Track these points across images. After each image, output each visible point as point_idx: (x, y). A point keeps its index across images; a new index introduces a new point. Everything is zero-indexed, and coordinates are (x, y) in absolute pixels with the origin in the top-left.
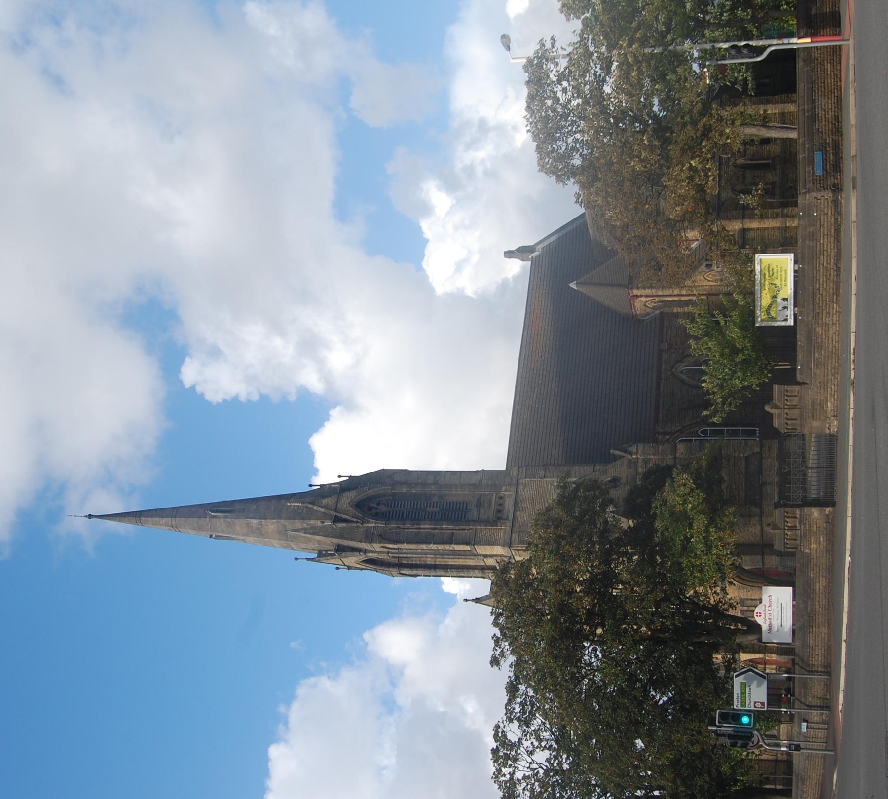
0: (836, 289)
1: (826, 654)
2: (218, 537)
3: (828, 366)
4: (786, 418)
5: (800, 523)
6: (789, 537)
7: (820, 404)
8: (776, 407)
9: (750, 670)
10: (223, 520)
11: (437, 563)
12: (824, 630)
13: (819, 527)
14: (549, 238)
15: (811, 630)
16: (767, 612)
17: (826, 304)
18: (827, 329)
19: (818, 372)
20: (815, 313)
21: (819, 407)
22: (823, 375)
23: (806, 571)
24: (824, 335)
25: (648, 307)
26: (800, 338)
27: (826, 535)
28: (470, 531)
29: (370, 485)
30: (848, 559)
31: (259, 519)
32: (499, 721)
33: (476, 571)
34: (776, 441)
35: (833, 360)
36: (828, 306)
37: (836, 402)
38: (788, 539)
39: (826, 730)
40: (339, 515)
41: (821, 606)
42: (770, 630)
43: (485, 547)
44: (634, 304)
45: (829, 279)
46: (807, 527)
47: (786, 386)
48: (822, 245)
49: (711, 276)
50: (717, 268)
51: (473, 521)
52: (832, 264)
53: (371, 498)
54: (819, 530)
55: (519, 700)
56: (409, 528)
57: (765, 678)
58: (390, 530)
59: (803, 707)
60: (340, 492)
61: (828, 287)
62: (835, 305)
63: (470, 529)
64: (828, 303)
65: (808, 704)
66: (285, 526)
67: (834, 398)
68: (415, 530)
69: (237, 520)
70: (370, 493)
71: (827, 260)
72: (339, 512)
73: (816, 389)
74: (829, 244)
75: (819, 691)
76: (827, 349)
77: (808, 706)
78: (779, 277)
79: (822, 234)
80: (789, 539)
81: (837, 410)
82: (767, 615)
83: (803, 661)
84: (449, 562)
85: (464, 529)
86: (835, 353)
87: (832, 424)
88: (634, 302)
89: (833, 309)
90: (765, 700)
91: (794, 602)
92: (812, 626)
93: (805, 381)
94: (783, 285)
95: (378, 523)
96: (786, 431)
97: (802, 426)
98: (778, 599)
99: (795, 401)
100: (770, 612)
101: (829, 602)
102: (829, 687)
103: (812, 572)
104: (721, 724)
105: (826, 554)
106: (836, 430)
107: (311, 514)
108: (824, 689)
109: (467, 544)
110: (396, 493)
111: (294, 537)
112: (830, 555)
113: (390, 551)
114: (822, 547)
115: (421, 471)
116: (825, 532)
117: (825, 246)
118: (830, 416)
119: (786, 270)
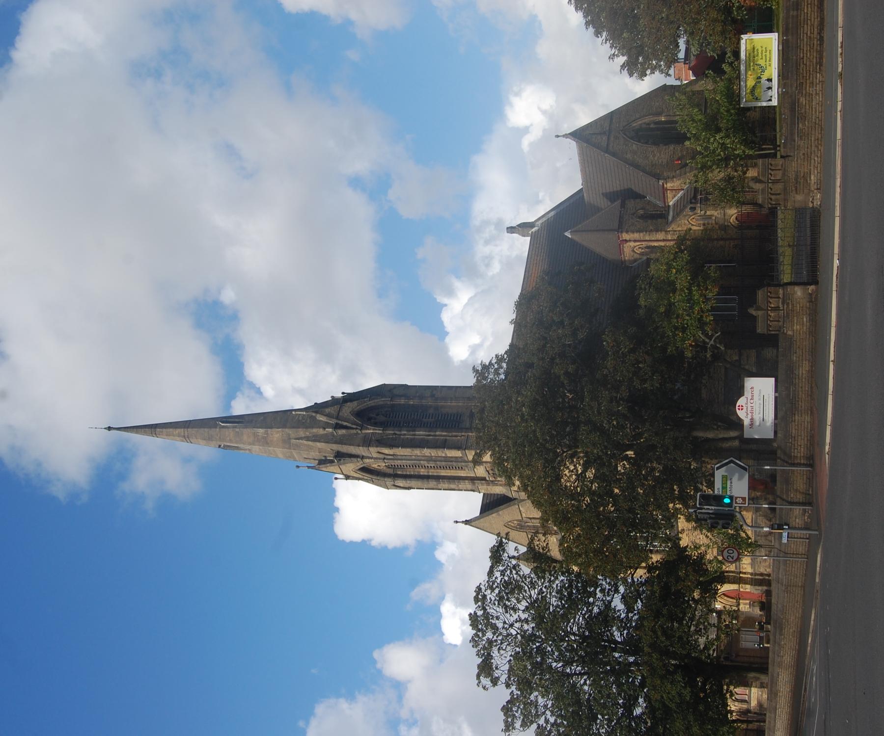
1: (809, 444)
2: (226, 447)
3: (811, 137)
4: (770, 193)
5: (783, 303)
7: (803, 177)
8: (759, 309)
9: (732, 462)
10: (232, 429)
11: (430, 474)
13: (802, 307)
14: (548, 214)
16: (749, 405)
17: (810, 74)
18: (811, 99)
20: (798, 83)
21: (802, 180)
22: (806, 146)
23: (789, 354)
24: (807, 105)
25: (636, 252)
26: (784, 111)
27: (809, 315)
28: (463, 437)
29: (370, 396)
30: (836, 262)
31: (265, 428)
33: (467, 481)
34: (754, 350)
35: (817, 131)
36: (811, 76)
37: (819, 174)
38: (771, 321)
39: (808, 539)
40: (340, 422)
42: (752, 424)
44: (623, 250)
45: (813, 49)
46: (790, 307)
47: (770, 160)
48: (805, 14)
49: (694, 220)
50: (701, 211)
51: (467, 429)
52: (816, 32)
53: (371, 409)
54: (802, 310)
55: (501, 568)
56: (406, 434)
57: (747, 471)
58: (387, 435)
59: (785, 503)
60: (342, 403)
61: (812, 57)
62: (818, 74)
63: (462, 436)
66: (289, 435)
67: (817, 170)
68: (411, 437)
69: (245, 430)
70: (370, 404)
71: (811, 29)
72: (339, 420)
73: (799, 161)
74: (813, 13)
75: (802, 486)
76: (810, 120)
77: (787, 502)
78: (764, 57)
79: (806, 4)
80: (772, 321)
81: (820, 183)
82: (749, 409)
85: (456, 436)
87: (815, 198)
88: (623, 246)
89: (816, 79)
91: (777, 394)
92: (795, 414)
93: (789, 154)
94: (768, 65)
95: (376, 430)
97: (786, 200)
98: (760, 390)
100: (752, 405)
103: (795, 355)
104: (702, 507)
106: (819, 203)
107: (314, 423)
108: (806, 484)
109: (458, 448)
110: (394, 404)
112: (813, 336)
114: (805, 328)
115: (419, 386)
117: (809, 15)
118: (813, 190)
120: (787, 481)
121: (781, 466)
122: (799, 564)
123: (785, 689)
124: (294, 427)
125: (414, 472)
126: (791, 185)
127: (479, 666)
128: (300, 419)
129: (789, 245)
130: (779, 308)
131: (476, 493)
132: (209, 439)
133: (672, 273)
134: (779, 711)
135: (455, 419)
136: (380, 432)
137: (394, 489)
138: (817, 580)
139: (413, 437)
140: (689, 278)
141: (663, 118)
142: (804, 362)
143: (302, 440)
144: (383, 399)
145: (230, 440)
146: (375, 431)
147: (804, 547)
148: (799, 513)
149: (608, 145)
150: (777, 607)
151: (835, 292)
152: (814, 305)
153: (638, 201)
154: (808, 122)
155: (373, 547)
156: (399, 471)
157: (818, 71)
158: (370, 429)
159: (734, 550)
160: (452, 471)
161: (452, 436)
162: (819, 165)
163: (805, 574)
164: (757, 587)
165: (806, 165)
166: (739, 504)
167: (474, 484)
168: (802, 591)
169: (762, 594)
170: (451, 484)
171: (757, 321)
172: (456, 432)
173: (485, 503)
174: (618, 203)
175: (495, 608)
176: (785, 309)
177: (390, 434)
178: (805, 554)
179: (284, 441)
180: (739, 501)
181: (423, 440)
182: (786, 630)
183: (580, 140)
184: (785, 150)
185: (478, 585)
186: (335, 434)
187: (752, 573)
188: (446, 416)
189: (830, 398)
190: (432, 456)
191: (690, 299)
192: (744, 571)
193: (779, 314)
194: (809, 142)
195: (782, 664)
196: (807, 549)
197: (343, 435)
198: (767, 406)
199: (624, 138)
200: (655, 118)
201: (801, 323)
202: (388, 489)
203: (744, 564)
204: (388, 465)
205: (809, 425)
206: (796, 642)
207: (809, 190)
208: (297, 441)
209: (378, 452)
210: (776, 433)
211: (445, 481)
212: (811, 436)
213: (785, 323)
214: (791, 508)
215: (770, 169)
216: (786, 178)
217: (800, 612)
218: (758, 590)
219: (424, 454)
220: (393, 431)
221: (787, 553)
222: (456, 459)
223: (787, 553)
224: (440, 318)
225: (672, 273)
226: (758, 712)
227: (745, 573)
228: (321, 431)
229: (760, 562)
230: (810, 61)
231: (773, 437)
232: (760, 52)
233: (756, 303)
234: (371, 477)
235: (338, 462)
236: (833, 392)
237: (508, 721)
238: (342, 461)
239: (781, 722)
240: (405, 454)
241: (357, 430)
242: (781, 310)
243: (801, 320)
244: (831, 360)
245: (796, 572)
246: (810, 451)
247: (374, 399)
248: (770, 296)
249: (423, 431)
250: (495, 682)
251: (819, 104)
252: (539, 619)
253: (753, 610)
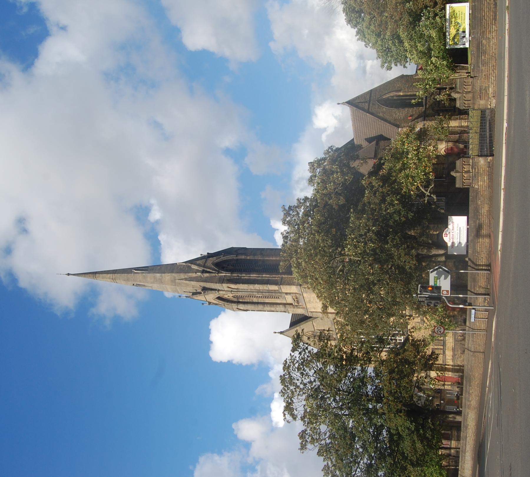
0: (495, 16)
1: (488, 257)
2: (138, 285)
3: (490, 65)
5: (472, 168)
6: (465, 178)
7: (485, 89)
8: (457, 172)
10: (141, 274)
11: (259, 301)
12: (486, 240)
15: (478, 241)
17: (489, 26)
18: (489, 41)
19: (483, 68)
20: (482, 31)
22: (486, 70)
27: (488, 175)
28: (279, 278)
29: (224, 254)
30: (505, 125)
36: (489, 27)
37: (494, 88)
38: (464, 179)
39: (487, 319)
40: (205, 269)
41: (485, 224)
43: (287, 286)
46: (477, 170)
54: (484, 172)
56: (244, 276)
58: (233, 277)
59: (471, 330)
61: (490, 15)
62: (494, 26)
63: (279, 277)
64: (490, 25)
65: (476, 292)
66: (175, 277)
67: (493, 85)
68: (248, 278)
69: (149, 274)
72: (205, 268)
73: (482, 79)
75: (483, 283)
78: (461, 18)
80: (466, 180)
81: (495, 93)
82: (451, 236)
83: (473, 262)
84: (266, 300)
86: (494, 57)
87: (492, 102)
89: (493, 28)
90: (449, 289)
91: (468, 227)
93: (475, 76)
95: (227, 273)
96: (464, 108)
97: (474, 104)
98: (458, 224)
99: (469, 89)
101: (490, 221)
102: (489, 280)
103: (479, 200)
105: (488, 189)
106: (494, 106)
107: (190, 270)
111: (179, 283)
112: (490, 189)
113: (233, 290)
115: (253, 248)
116: (488, 174)
119: (464, 14)
120: (474, 280)
124: (178, 273)
125: (250, 300)
128: (182, 268)
134: (468, 439)
135: (275, 268)
137: (238, 311)
138: (493, 340)
139: (249, 278)
142: (485, 205)
144: (232, 256)
145: (140, 280)
146: (226, 274)
147: (484, 324)
154: (488, 55)
155: (234, 364)
157: (494, 24)
158: (223, 273)
159: (441, 327)
160: (272, 299)
161: (272, 277)
164: (456, 374)
166: (445, 294)
172: (275, 275)
173: (292, 321)
175: (295, 373)
179: (172, 281)
180: (445, 292)
182: (473, 383)
183: (352, 106)
184: (474, 73)
185: (285, 359)
186: (202, 276)
190: (260, 290)
192: (448, 364)
194: (488, 67)
195: (470, 406)
197: (207, 277)
199: (378, 104)
200: (397, 93)
201: (483, 181)
202: (234, 311)
205: (488, 244)
207: (488, 97)
209: (228, 287)
210: (467, 252)
212: (489, 252)
215: (465, 85)
216: (474, 90)
217: (482, 370)
218: (456, 375)
219: (256, 288)
222: (275, 291)
224: (274, 238)
226: (456, 455)
227: (448, 365)
228: (194, 275)
230: (489, 18)
231: (465, 254)
232: (458, 14)
233: (456, 168)
236: (503, 209)
237: (302, 444)
238: (206, 293)
240: (244, 288)
243: (483, 179)
244: (502, 188)
245: (479, 342)
247: (226, 256)
249: (255, 274)
250: (294, 417)
251: (494, 44)
252: (322, 379)
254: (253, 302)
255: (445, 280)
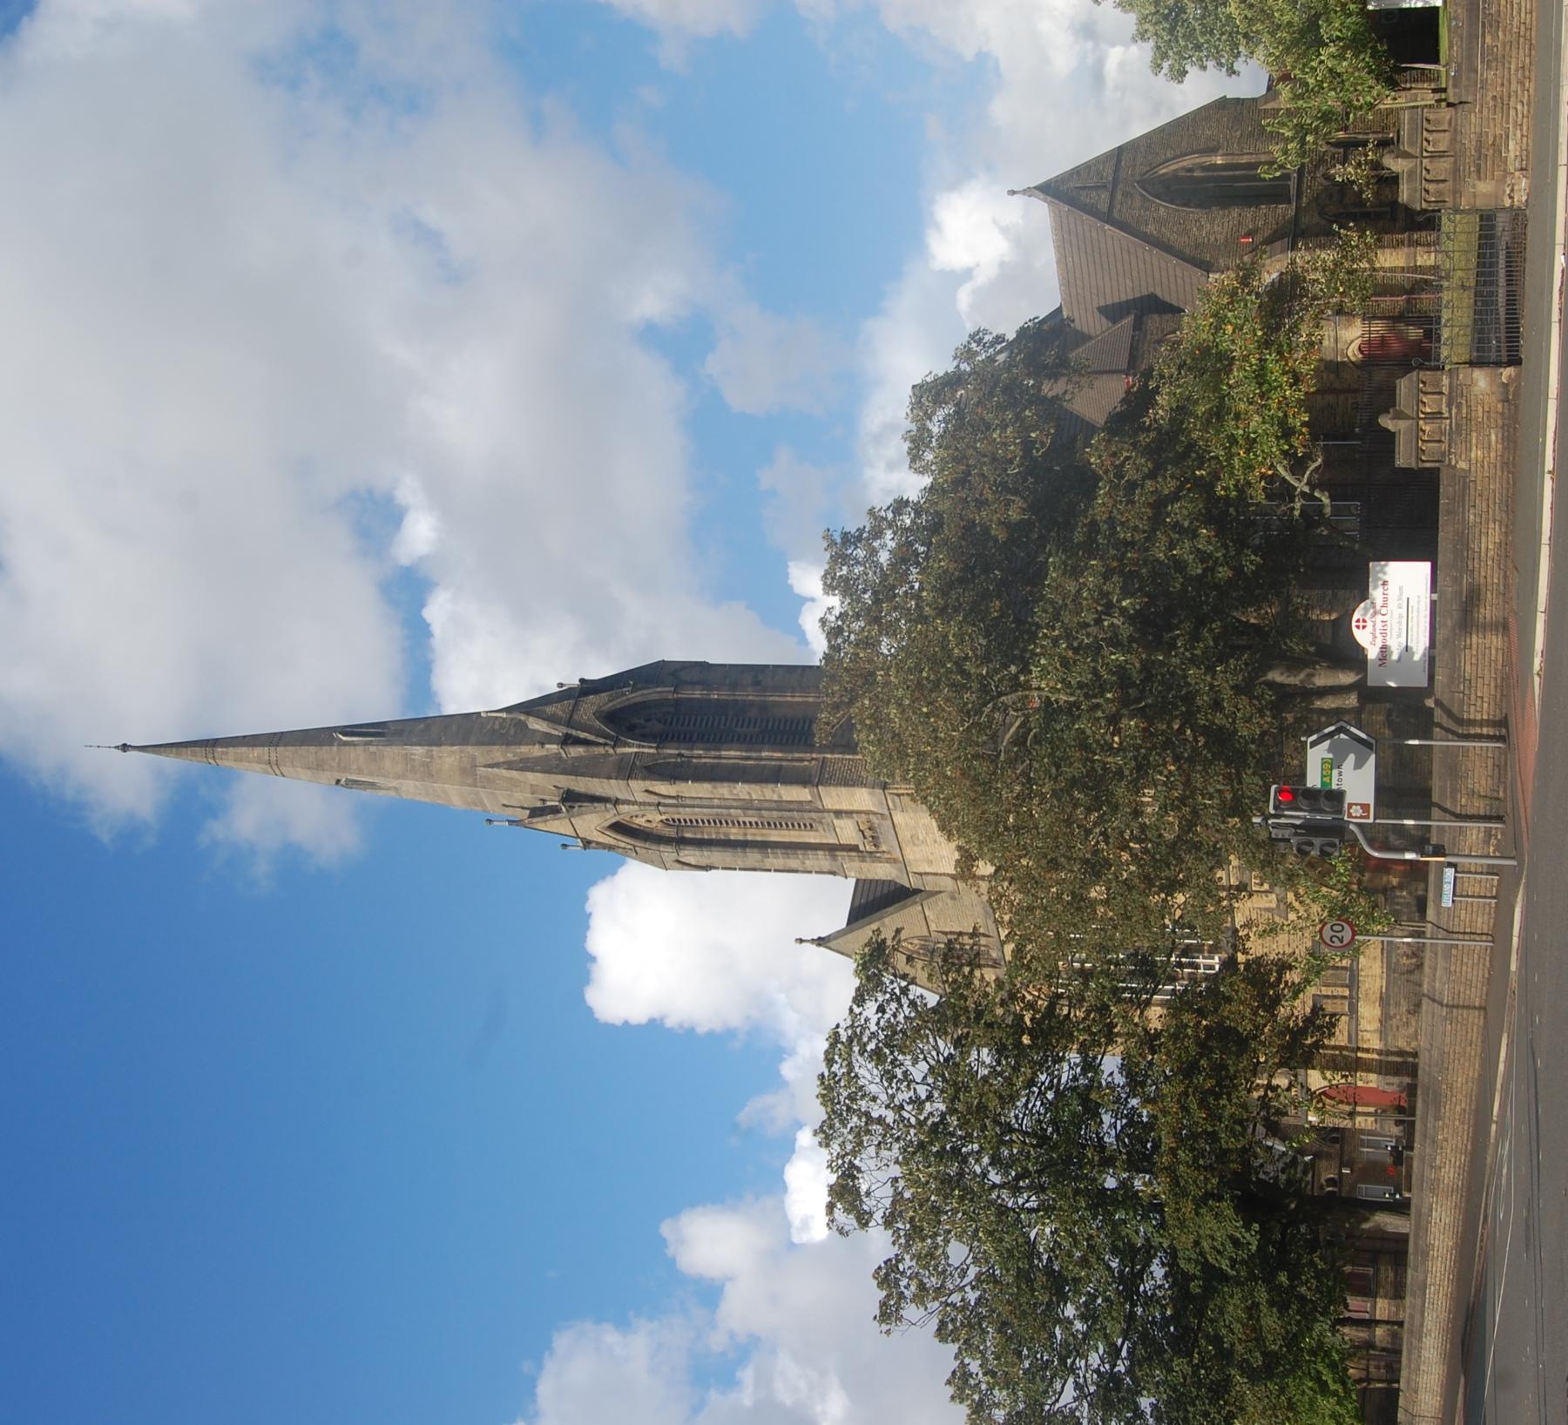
2: (351, 784)
3: (1510, 63)
5: (1449, 405)
7: (1493, 144)
8: (1400, 416)
10: (362, 748)
11: (749, 838)
15: (1468, 642)
22: (1499, 81)
27: (1503, 428)
28: (813, 762)
31: (428, 745)
32: (838, 1026)
37: (1525, 139)
38: (1423, 441)
40: (574, 732)
46: (1464, 411)
54: (1488, 418)
56: (701, 755)
63: (813, 759)
66: (474, 758)
67: (1521, 130)
68: (712, 761)
69: (388, 748)
72: (572, 728)
73: (1485, 112)
75: (1483, 782)
76: (1509, 27)
81: (1527, 156)
82: (1379, 626)
85: (802, 760)
87: (1516, 188)
91: (1435, 597)
93: (1463, 100)
95: (643, 747)
96: (1424, 205)
97: (1457, 192)
98: (1401, 588)
100: (1384, 618)
103: (1472, 511)
105: (1503, 472)
106: (1524, 198)
114: (1493, 455)
115: (730, 665)
116: (1500, 422)
118: (1512, 171)
120: (1454, 771)
121: (1441, 740)
122: (1476, 956)
123: (1443, 1241)
125: (717, 833)
126: (1467, 161)
127: (831, 1188)
128: (497, 727)
129: (1462, 285)
130: (1442, 413)
131: (839, 879)
132: (319, 766)
133: (1224, 334)
136: (652, 751)
138: (1513, 967)
140: (1260, 333)
141: (1219, 158)
142: (1491, 525)
143: (498, 768)
144: (659, 689)
146: (641, 750)
147: (1486, 917)
148: (1477, 838)
149: (1111, 207)
150: (1431, 1056)
151: (1557, 324)
152: (1512, 407)
153: (1168, 316)
154: (1504, 32)
156: (687, 832)
160: (792, 832)
161: (793, 760)
162: (1525, 120)
163: (1488, 979)
164: (1391, 1079)
165: (1498, 121)
166: (1356, 817)
167: (834, 857)
168: (1482, 1017)
169: (1402, 1092)
170: (789, 858)
171: (1397, 443)
172: (801, 752)
173: (857, 904)
174: (1128, 321)
176: (1453, 415)
177: (671, 756)
178: (1487, 934)
181: (735, 768)
186: (564, 756)
187: (1381, 1051)
188: (783, 724)
189: (1545, 552)
190: (751, 800)
191: (1260, 376)
192: (1365, 1046)
193: (1440, 427)
194: (1506, 72)
195: (1438, 1185)
196: (1492, 921)
197: (579, 758)
198: (1415, 629)
200: (1204, 159)
203: (1366, 1031)
204: (667, 820)
206: (1468, 1134)
207: (1505, 171)
208: (490, 769)
209: (647, 791)
210: (1431, 678)
211: (778, 851)
213: (1453, 445)
214: (1460, 827)
220: (677, 749)
221: (1453, 932)
222: (800, 806)
223: (1453, 932)
225: (1224, 334)
226: (1389, 1346)
228: (536, 751)
229: (1398, 1027)
234: (632, 842)
235: (568, 811)
239: (1435, 1316)
241: (607, 748)
242: (1446, 418)
244: (1546, 470)
246: (1501, 710)
247: (640, 689)
248: (1424, 389)
249: (736, 750)
250: (863, 1220)
253: (1381, 1127)
254: (730, 840)
255: (1357, 771)
